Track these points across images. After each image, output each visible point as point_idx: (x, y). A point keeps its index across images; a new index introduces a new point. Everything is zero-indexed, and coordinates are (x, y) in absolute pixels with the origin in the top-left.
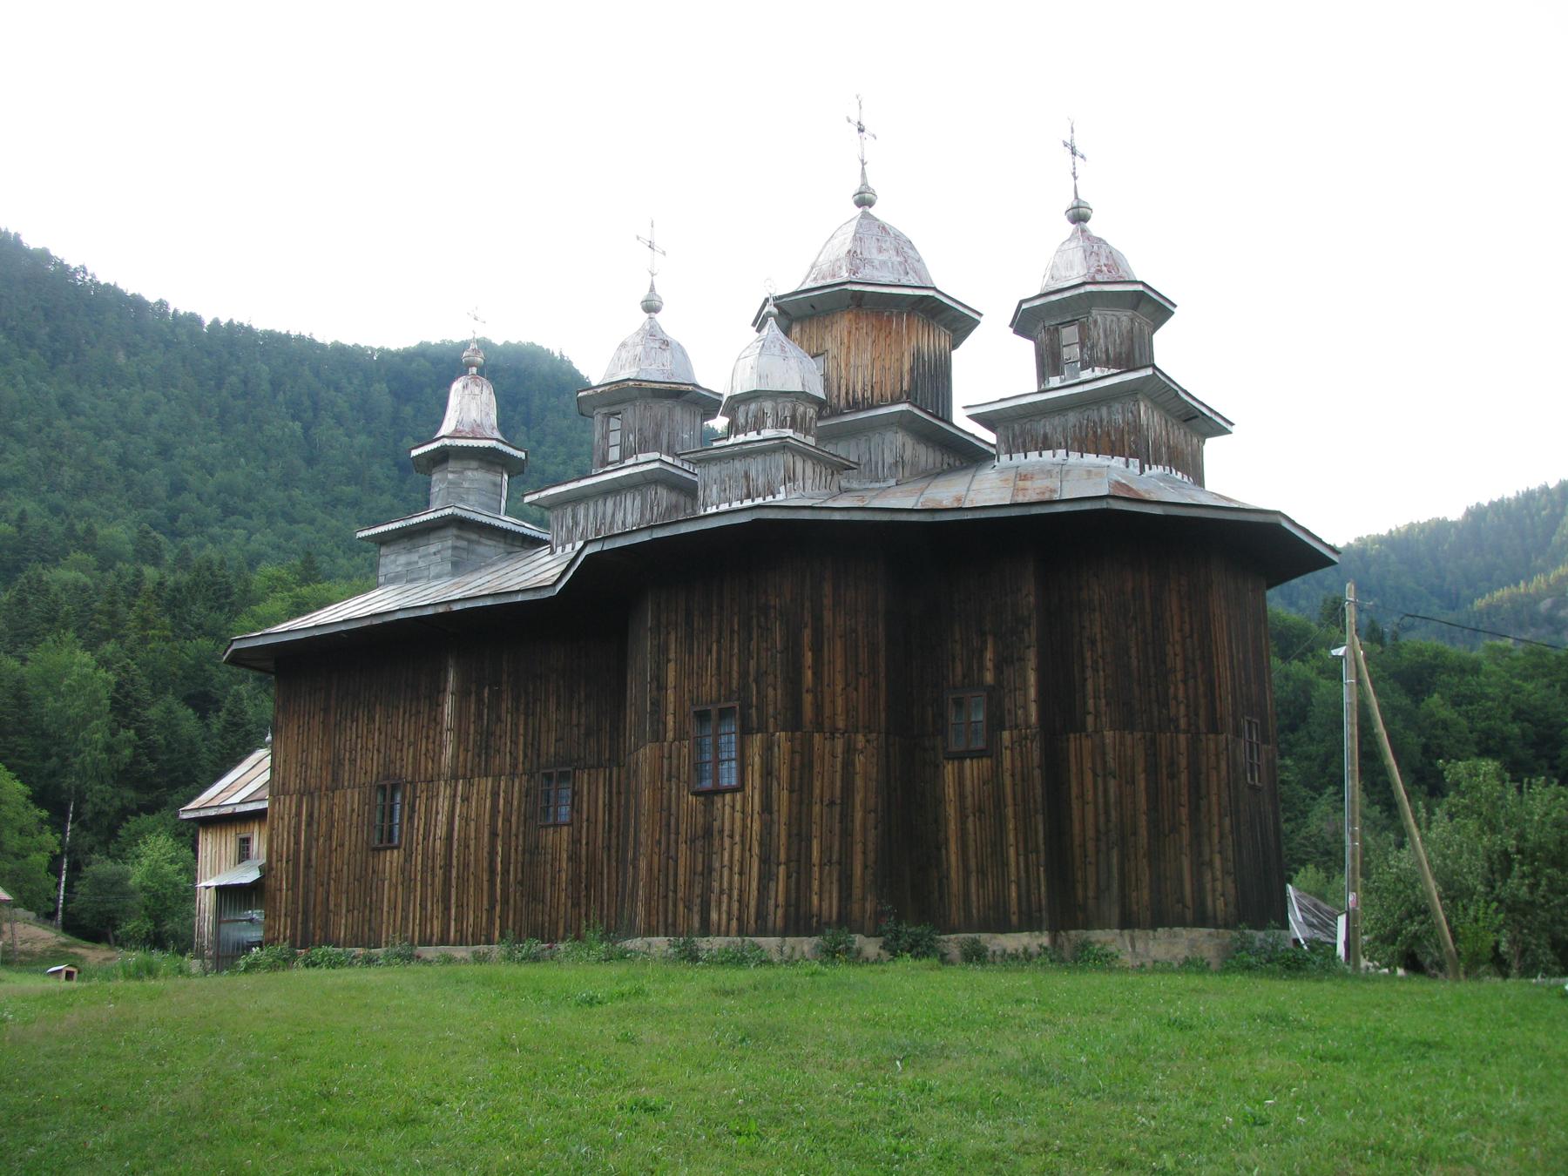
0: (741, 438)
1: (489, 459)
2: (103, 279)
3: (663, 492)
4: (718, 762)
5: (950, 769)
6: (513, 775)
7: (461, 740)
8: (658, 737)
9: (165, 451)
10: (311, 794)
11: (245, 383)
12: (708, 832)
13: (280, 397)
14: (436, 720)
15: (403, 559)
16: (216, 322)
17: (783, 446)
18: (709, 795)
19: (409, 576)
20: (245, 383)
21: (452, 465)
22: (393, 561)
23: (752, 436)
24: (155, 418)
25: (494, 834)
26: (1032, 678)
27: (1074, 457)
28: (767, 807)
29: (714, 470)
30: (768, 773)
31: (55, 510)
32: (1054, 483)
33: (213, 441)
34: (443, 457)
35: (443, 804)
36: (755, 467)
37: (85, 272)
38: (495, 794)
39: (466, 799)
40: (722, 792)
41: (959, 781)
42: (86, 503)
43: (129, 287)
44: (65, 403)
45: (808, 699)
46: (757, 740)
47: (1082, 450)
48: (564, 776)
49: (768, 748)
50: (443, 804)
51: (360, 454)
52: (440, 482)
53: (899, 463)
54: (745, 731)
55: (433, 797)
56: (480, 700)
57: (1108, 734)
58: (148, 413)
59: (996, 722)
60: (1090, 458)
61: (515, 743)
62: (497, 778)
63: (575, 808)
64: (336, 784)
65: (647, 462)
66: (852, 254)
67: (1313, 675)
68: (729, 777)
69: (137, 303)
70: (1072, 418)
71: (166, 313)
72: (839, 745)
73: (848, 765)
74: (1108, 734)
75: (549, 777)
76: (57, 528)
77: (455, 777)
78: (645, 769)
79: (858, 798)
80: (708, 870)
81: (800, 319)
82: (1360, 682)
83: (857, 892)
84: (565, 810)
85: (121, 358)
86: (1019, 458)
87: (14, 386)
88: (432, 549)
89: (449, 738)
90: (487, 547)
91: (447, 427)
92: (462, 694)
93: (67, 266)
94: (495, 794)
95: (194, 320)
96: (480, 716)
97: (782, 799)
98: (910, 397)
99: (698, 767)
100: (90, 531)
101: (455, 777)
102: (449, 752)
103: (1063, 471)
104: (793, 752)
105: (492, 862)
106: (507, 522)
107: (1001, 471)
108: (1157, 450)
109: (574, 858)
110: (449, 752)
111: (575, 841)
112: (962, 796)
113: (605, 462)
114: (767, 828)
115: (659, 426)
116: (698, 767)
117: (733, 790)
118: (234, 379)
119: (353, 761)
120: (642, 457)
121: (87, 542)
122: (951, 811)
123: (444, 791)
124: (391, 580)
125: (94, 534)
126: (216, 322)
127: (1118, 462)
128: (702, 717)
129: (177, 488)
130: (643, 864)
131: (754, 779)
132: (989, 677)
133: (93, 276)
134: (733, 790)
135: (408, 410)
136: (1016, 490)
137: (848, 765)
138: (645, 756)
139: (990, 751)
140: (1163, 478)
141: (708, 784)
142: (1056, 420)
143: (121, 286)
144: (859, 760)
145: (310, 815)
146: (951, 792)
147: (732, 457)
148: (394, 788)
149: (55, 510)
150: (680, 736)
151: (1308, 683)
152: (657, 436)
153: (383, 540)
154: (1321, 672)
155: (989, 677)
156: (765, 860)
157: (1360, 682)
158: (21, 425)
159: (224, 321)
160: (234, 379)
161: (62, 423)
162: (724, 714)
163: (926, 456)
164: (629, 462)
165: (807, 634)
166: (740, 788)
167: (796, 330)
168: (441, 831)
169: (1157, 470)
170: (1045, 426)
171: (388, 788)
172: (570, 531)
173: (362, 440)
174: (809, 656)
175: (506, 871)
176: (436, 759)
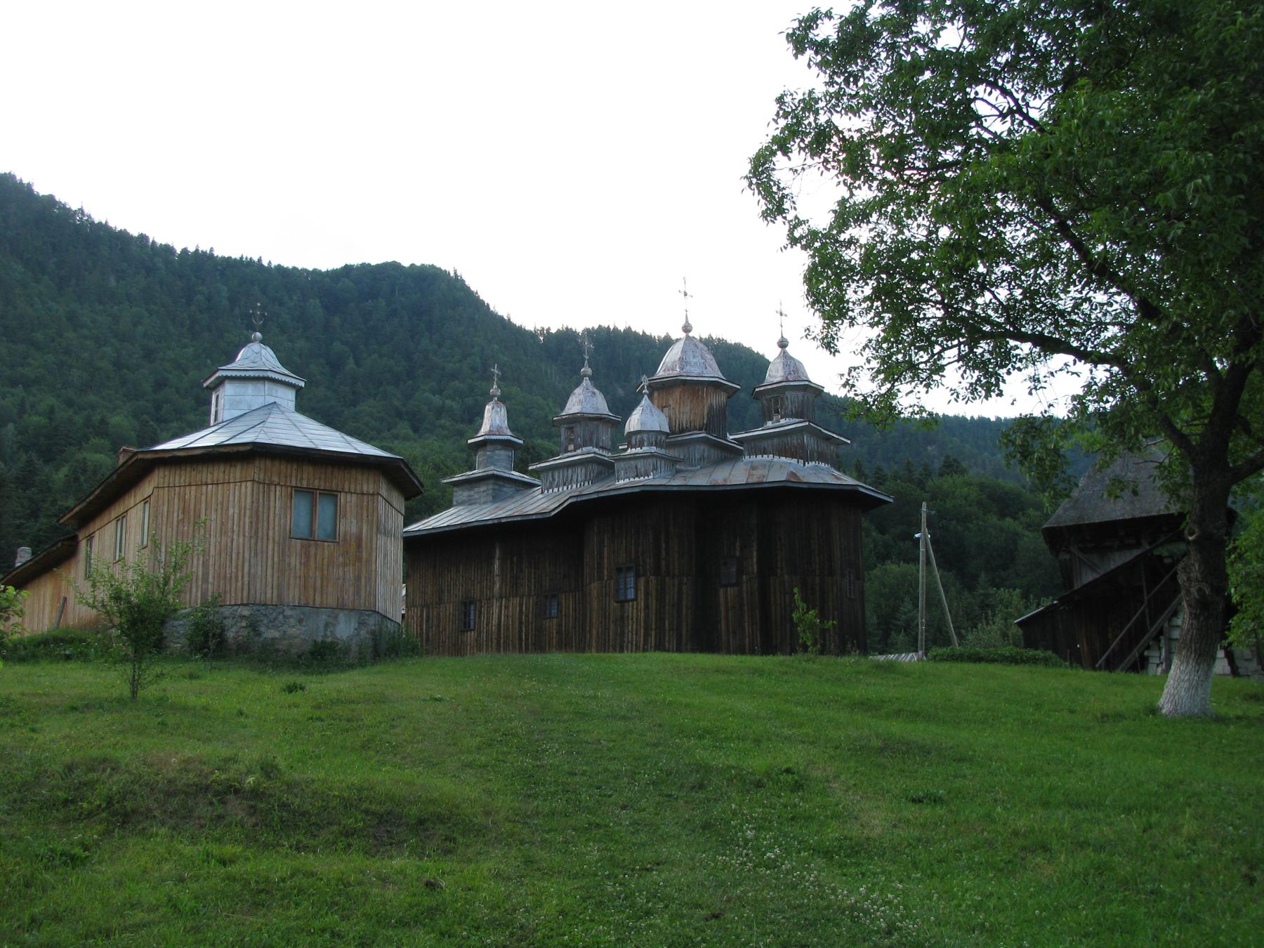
0: (634, 451)
1: (507, 444)
2: (98, 218)
3: (595, 466)
4: (626, 589)
5: (722, 591)
6: (529, 596)
7: (503, 581)
8: (600, 578)
9: (149, 354)
10: (428, 607)
11: (209, 300)
12: (622, 619)
13: (237, 311)
14: (491, 572)
15: (466, 493)
16: (185, 251)
17: (652, 455)
18: (623, 603)
19: (469, 502)
20: (209, 300)
21: (489, 447)
22: (460, 494)
23: (638, 450)
24: (140, 329)
25: (521, 623)
26: (755, 554)
27: (776, 458)
28: (647, 607)
29: (622, 464)
30: (647, 593)
31: (70, 403)
32: (765, 472)
33: (186, 347)
34: (483, 444)
35: (496, 610)
36: (640, 464)
37: (83, 213)
38: (521, 605)
39: (506, 607)
40: (629, 601)
41: (726, 596)
42: (92, 397)
43: (117, 224)
44: (72, 317)
45: (663, 562)
46: (642, 580)
47: (780, 456)
48: (554, 596)
49: (647, 583)
50: (496, 610)
51: (300, 356)
52: (480, 457)
53: (702, 459)
54: (637, 576)
55: (490, 607)
56: (512, 563)
57: (786, 577)
58: (135, 325)
59: (740, 572)
60: (783, 459)
61: (529, 581)
62: (522, 597)
63: (560, 611)
64: (440, 601)
65: (588, 452)
66: (681, 359)
67: (1020, 529)
68: (631, 595)
69: (123, 236)
70: (776, 441)
71: (147, 246)
72: (676, 582)
73: (680, 590)
74: (786, 577)
75: (546, 597)
76: (79, 419)
77: (501, 597)
78: (595, 593)
79: (684, 603)
80: (623, 633)
81: (658, 389)
82: (927, 551)
83: (684, 641)
84: (554, 611)
85: (112, 282)
86: (753, 458)
87: (32, 305)
88: (482, 489)
89: (497, 579)
90: (508, 489)
91: (485, 428)
92: (503, 560)
93: (69, 210)
94: (521, 605)
95: (168, 250)
96: (512, 569)
97: (653, 603)
98: (706, 428)
99: (617, 591)
100: (103, 421)
101: (501, 597)
102: (497, 586)
103: (770, 465)
104: (369, 561)
105: (520, 631)
106: (516, 475)
107: (746, 464)
108: (812, 454)
109: (559, 632)
110: (497, 586)
111: (560, 625)
112: (727, 603)
113: (567, 451)
114: (647, 616)
115: (592, 434)
116: (617, 591)
117: (632, 600)
118: (199, 297)
119: (449, 591)
120: (585, 449)
121: (102, 429)
122: (722, 608)
123: (496, 604)
124: (459, 504)
125: (107, 424)
126: (185, 251)
127: (794, 461)
128: (619, 570)
129: (160, 385)
130: (594, 632)
131: (641, 596)
132: (738, 553)
133: (89, 216)
134: (632, 600)
135: (337, 320)
136: (750, 475)
137: (680, 590)
138: (594, 588)
139: (738, 584)
140: (815, 468)
141: (622, 598)
142: (769, 442)
143: (112, 224)
144: (684, 587)
145: (428, 617)
146: (722, 600)
147: (630, 459)
148: (471, 603)
149: (70, 403)
150: (610, 578)
151: (1016, 534)
152: (591, 439)
153: (456, 484)
154: (1028, 526)
155: (738, 553)
156: (646, 629)
157: (927, 551)
158: (39, 336)
159: (192, 249)
160: (199, 297)
161: (70, 334)
162: (629, 569)
163: (714, 454)
164: (579, 451)
165: (663, 537)
166: (636, 599)
167: (656, 394)
168: (495, 622)
169: (812, 464)
170: (765, 444)
171: (467, 603)
172: (551, 484)
173: (301, 344)
174: (664, 545)
175: (527, 639)
176: (491, 589)
